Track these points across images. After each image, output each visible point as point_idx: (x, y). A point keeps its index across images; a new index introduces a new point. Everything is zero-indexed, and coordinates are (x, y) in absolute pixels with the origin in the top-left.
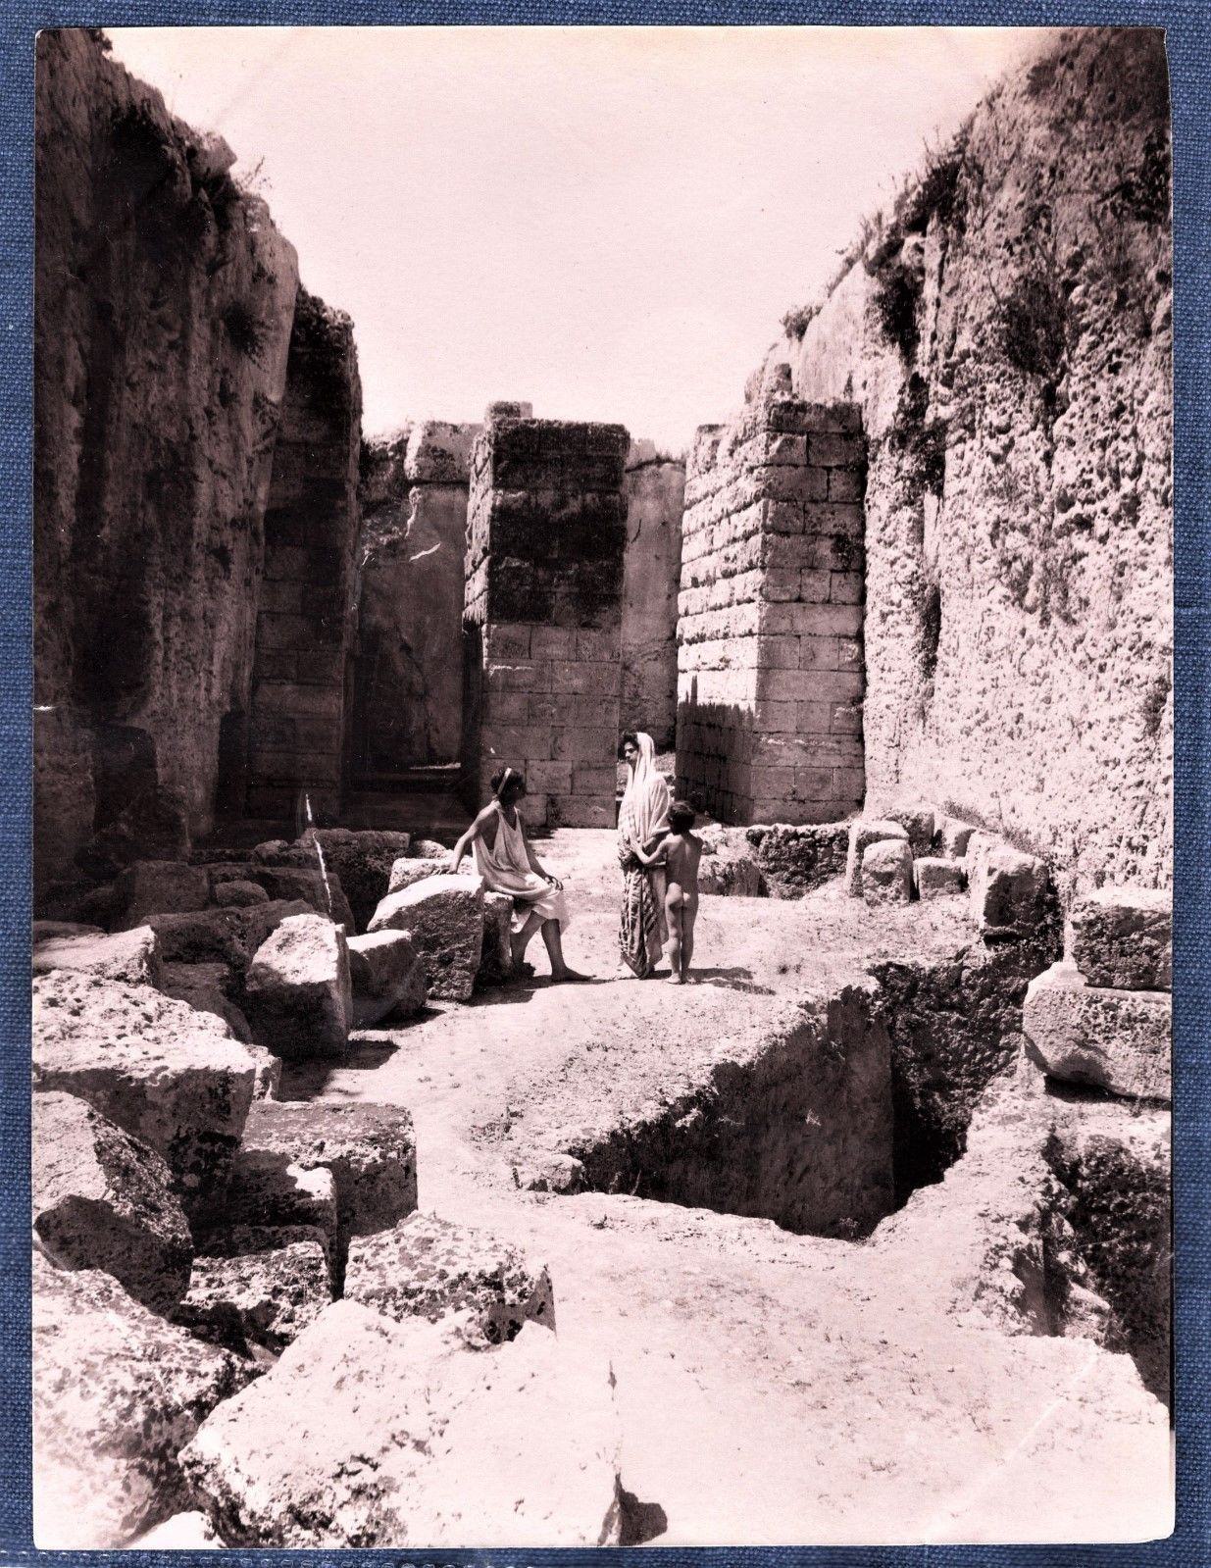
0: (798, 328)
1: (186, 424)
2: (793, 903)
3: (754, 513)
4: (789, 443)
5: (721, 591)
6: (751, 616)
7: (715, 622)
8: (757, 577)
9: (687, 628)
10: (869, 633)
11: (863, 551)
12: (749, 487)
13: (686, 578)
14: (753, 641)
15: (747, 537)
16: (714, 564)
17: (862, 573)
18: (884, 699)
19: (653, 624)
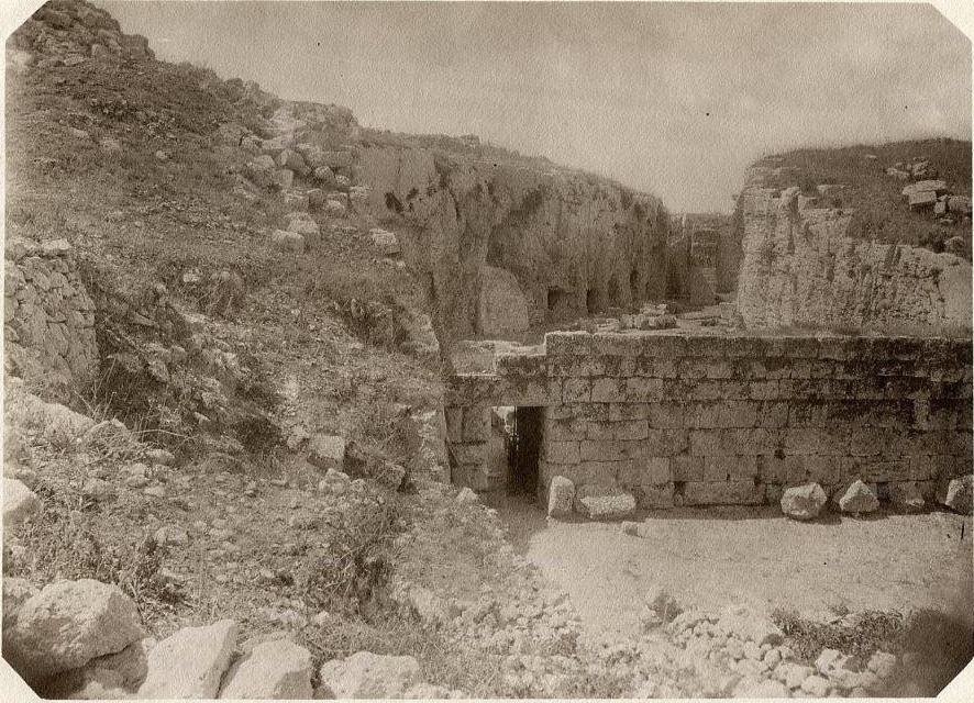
19: (550, 233)
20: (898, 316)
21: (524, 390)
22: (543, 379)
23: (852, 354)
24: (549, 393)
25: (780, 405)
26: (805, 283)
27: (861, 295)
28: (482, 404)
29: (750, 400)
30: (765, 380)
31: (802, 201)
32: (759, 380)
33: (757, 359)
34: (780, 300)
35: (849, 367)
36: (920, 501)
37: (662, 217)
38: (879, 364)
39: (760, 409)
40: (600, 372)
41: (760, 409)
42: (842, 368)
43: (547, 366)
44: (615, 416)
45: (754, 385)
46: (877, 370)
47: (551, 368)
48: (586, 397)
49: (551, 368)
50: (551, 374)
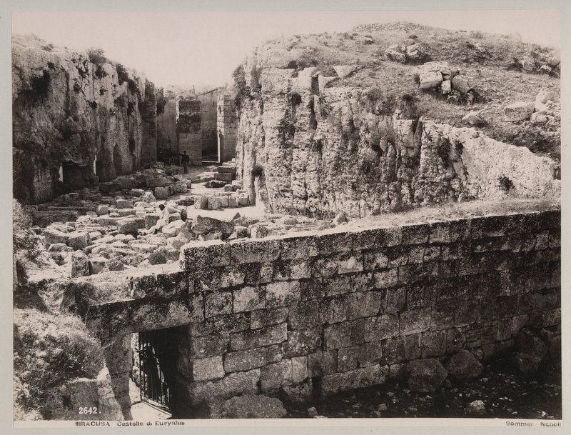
19: (58, 110)
20: (422, 183)
21: (165, 311)
22: (185, 298)
23: (456, 236)
24: (191, 309)
25: (400, 290)
26: (329, 154)
27: (386, 165)
28: (122, 332)
29: (375, 289)
30: (386, 269)
31: (322, 80)
32: (381, 270)
33: (378, 250)
34: (305, 170)
35: (453, 246)
36: (48, 285)
37: (149, 88)
38: (476, 243)
39: (383, 297)
40: (241, 281)
41: (383, 297)
42: (448, 250)
43: (187, 281)
44: (256, 324)
45: (380, 276)
46: (473, 249)
47: (191, 283)
48: (227, 309)
49: (191, 283)
50: (191, 289)
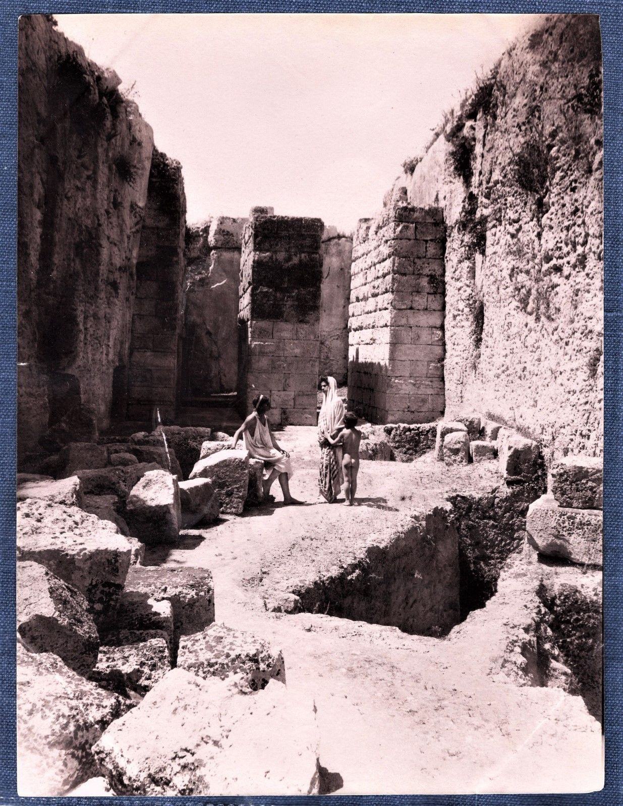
0: (411, 168)
1: (96, 218)
2: (408, 464)
3: (388, 264)
4: (406, 228)
5: (371, 304)
6: (387, 317)
7: (368, 320)
8: (389, 296)
9: (353, 323)
10: (447, 326)
11: (444, 283)
12: (385, 250)
13: (353, 297)
14: (387, 330)
15: (384, 276)
16: (367, 290)
17: (444, 294)
18: (455, 359)
19: (336, 321)
